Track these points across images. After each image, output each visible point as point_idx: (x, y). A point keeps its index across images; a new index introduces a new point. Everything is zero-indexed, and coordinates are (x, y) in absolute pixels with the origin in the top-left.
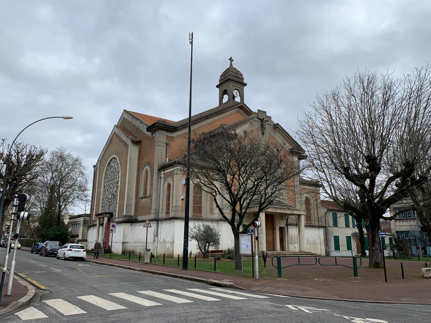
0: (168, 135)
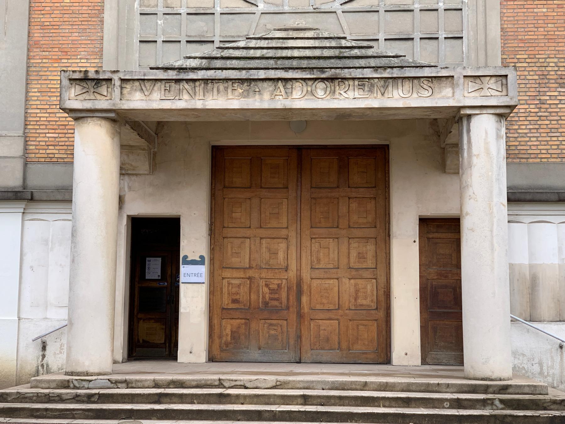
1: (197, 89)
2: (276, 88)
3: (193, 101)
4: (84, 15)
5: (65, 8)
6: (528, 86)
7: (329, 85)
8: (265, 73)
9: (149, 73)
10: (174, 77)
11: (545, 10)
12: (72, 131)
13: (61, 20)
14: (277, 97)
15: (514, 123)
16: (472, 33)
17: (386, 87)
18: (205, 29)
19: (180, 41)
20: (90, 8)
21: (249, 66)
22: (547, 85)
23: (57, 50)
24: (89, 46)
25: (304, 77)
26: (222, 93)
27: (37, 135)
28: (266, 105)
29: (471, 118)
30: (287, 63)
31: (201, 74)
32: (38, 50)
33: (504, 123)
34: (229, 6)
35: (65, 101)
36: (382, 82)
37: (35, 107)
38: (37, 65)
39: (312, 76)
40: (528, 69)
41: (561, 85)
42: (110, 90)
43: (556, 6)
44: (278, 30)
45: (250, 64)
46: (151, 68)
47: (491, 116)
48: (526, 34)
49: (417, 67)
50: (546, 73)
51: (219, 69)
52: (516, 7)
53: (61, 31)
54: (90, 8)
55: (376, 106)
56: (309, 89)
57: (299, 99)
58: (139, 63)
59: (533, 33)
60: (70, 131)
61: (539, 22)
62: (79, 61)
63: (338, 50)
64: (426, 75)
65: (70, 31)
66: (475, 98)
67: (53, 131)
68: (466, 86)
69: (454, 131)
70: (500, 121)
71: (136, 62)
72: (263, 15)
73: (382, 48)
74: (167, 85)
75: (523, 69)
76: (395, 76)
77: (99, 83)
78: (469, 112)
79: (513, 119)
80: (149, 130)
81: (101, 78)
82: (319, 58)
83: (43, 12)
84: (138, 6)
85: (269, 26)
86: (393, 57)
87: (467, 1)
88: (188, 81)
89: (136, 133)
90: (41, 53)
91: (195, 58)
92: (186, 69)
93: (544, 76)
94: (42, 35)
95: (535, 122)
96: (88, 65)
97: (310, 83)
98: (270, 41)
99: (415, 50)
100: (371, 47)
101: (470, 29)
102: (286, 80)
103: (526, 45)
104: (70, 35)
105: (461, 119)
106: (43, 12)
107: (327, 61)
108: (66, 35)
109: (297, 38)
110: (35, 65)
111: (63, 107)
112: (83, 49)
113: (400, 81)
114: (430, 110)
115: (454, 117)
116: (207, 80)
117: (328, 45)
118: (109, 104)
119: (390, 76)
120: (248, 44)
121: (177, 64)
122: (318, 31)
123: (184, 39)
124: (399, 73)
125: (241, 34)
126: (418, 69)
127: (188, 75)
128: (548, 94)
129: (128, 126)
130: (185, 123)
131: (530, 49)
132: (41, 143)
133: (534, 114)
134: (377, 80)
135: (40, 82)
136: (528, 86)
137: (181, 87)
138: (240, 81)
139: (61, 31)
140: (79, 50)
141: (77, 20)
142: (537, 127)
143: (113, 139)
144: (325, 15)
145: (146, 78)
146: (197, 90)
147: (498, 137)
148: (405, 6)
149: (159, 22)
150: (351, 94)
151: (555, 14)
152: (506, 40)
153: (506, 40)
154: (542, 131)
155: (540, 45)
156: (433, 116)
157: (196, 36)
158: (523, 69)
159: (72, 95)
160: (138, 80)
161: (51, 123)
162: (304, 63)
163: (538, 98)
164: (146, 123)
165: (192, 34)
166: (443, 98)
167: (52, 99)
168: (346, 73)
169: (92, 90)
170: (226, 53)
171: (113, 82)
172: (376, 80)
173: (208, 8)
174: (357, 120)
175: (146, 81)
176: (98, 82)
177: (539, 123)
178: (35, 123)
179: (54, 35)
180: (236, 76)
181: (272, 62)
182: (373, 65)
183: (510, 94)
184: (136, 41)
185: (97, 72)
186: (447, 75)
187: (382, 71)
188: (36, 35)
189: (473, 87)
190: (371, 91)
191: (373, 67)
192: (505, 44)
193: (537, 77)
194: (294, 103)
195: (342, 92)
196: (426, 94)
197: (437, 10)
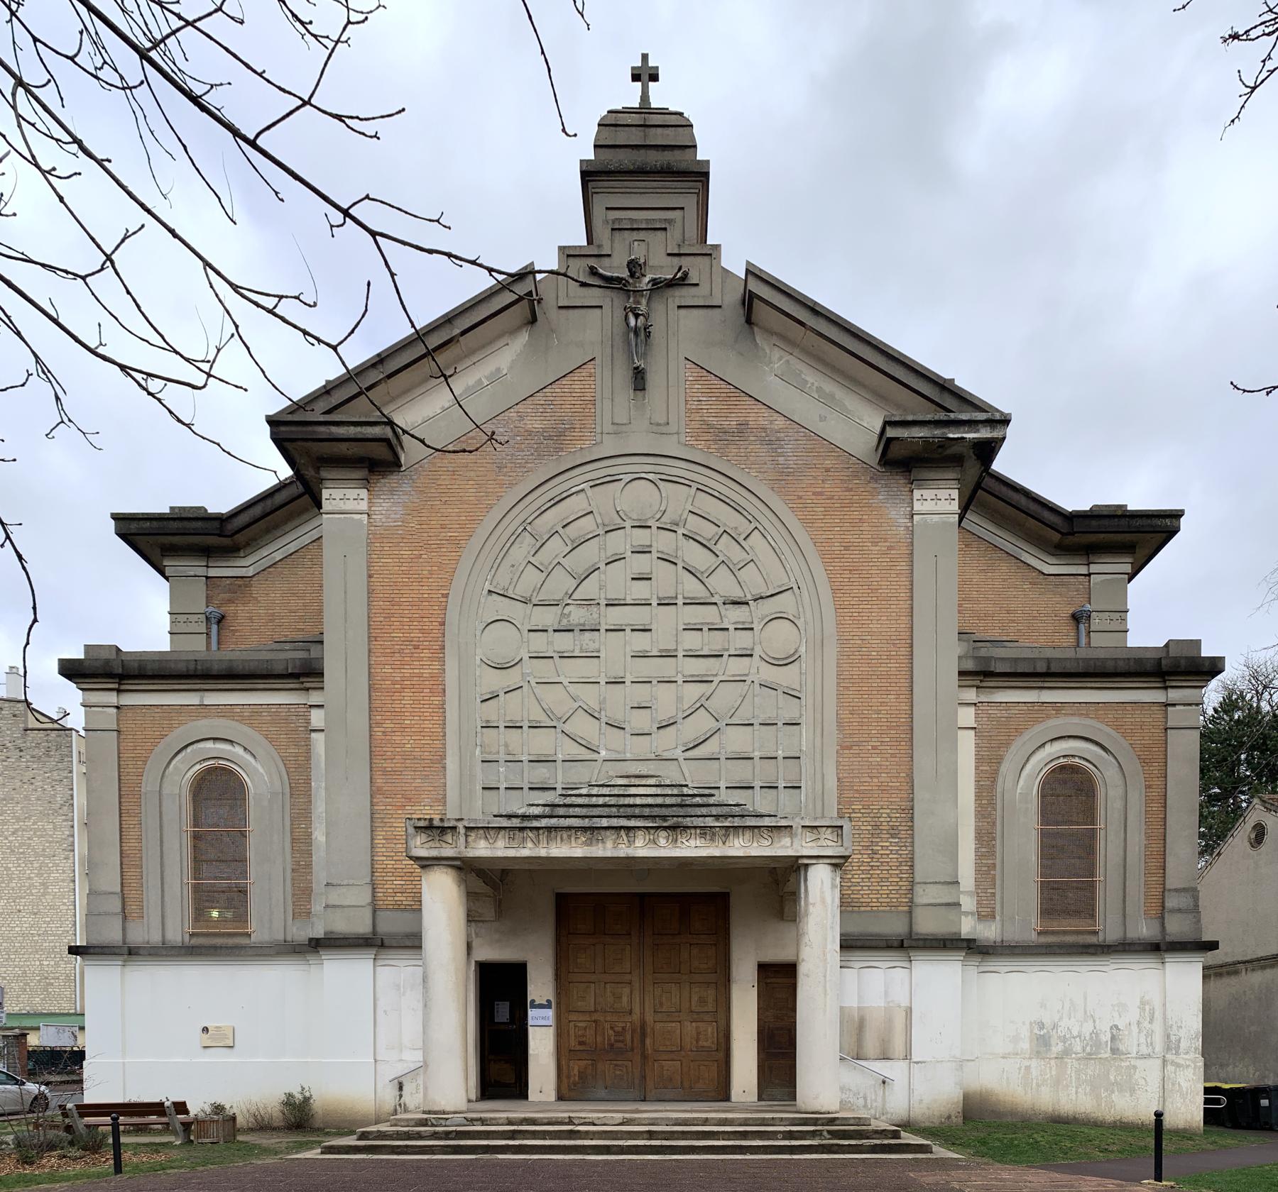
0: (212, 572)
2: (619, 837)
17: (727, 836)
28: (609, 854)
30: (629, 811)
31: (544, 822)
33: (839, 873)
57: (641, 848)
66: (812, 848)
71: (479, 809)
73: (723, 796)
78: (806, 861)
88: (531, 829)
93: (876, 827)
121: (520, 812)
123: (526, 787)
147: (833, 886)
150: (692, 843)
162: (647, 811)
168: (688, 822)
170: (568, 801)
176: (443, 830)
181: (614, 810)
184: (479, 788)
190: (712, 840)
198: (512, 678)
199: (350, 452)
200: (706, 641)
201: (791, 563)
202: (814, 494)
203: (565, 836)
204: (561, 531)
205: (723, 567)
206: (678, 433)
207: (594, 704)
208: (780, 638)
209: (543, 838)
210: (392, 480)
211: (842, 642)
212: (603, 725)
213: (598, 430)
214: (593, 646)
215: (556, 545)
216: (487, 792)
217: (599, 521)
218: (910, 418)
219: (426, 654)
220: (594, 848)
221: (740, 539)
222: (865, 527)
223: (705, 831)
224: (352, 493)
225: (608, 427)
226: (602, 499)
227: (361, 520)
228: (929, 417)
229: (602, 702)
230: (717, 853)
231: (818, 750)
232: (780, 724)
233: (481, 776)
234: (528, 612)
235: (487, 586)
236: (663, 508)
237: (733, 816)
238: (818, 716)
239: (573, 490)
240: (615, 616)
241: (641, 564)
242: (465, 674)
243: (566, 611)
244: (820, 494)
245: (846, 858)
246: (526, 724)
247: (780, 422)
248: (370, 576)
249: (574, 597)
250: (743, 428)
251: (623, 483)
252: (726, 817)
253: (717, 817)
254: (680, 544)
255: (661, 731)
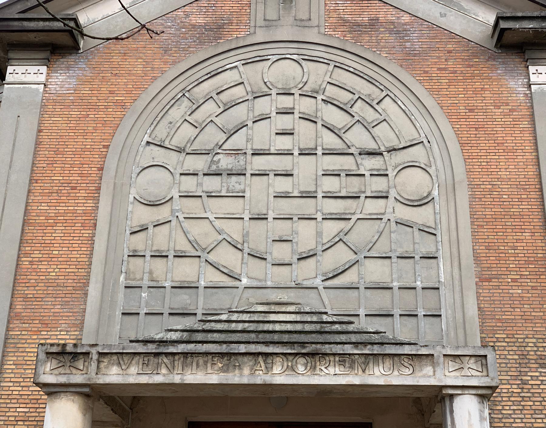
1: (176, 363)
2: (256, 363)
3: (171, 376)
4: (68, 288)
5: (50, 281)
6: (509, 365)
7: (309, 361)
8: (246, 348)
9: (129, 346)
10: (154, 351)
11: (520, 291)
12: (43, 406)
13: (45, 292)
14: (257, 372)
15: (497, 403)
16: (450, 312)
17: (366, 364)
18: (188, 301)
19: (163, 314)
20: (75, 281)
21: (230, 340)
22: (528, 365)
23: (38, 322)
24: (70, 318)
25: (285, 352)
26: (201, 368)
27: (7, 410)
28: (245, 381)
29: (453, 398)
30: (268, 337)
31: (181, 348)
32: (18, 322)
33: (486, 404)
34: (212, 280)
35: (39, 375)
36: (363, 359)
37: (8, 380)
38: (16, 337)
39: (293, 351)
40: (507, 349)
41: (542, 366)
42: (86, 364)
43: (530, 288)
44: (261, 304)
45: (231, 337)
46: (131, 341)
47: (473, 397)
48: (503, 314)
49: (397, 344)
50: (525, 353)
51: (199, 342)
52: (491, 287)
53: (43, 303)
54: (75, 281)
55: (358, 383)
56: (290, 364)
57: (279, 375)
58: (120, 334)
59: (509, 313)
60: (41, 406)
61: (515, 302)
62: (58, 333)
63: (319, 325)
64: (406, 353)
65: (53, 303)
66: (456, 377)
67: (24, 406)
68: (446, 365)
69: (437, 410)
70: (483, 402)
71: (115, 336)
72: (246, 289)
73: (363, 323)
74: (146, 359)
75: (503, 348)
76: (375, 352)
77: (76, 357)
78: (451, 392)
79: (496, 399)
80: (124, 404)
81: (79, 351)
82: (300, 332)
83: (27, 285)
84: (124, 280)
85: (252, 300)
86: (374, 333)
87: (443, 281)
88: (167, 354)
89: (109, 408)
90: (21, 325)
91: (176, 331)
92: (166, 342)
93: (523, 356)
94: (24, 307)
95: (518, 403)
96: (68, 337)
97: (290, 358)
98: (252, 314)
99: (395, 326)
100: (352, 323)
101: (448, 308)
102: (266, 355)
103: (505, 325)
104: (52, 307)
105: (443, 399)
106: (27, 285)
107: (308, 336)
108: (48, 307)
109: (279, 312)
110: (13, 337)
111: (37, 381)
112: (64, 322)
113: (380, 358)
114: (411, 388)
115: (437, 396)
116: (187, 353)
117: (309, 320)
118: (84, 379)
119: (371, 353)
120: (230, 317)
121: (158, 337)
122: (299, 306)
123: (166, 311)
124: (380, 350)
125: (224, 307)
126: (398, 347)
127: (168, 349)
128: (529, 374)
129: (101, 401)
130: (162, 398)
131: (508, 329)
132: (10, 419)
133: (517, 395)
134: (358, 356)
135: (16, 354)
136: (509, 365)
137: (160, 361)
138: (220, 355)
139: (43, 303)
140: (60, 322)
141: (61, 292)
142: (520, 408)
143: (85, 415)
144: (307, 290)
145: (124, 351)
146: (176, 364)
147: (482, 419)
148: (385, 284)
149: (143, 295)
150: (331, 370)
151: (530, 295)
152: (484, 319)
153: (484, 319)
154: (526, 412)
155: (518, 325)
156: (416, 395)
157: (178, 309)
158: (503, 348)
159: (48, 369)
160: (116, 353)
161: (23, 397)
162: (286, 338)
163: (520, 378)
164: (121, 398)
165: (175, 307)
166: (424, 376)
167: (27, 372)
168: (327, 349)
169: (68, 364)
170: (207, 326)
171: (90, 356)
172: (357, 357)
173: (193, 282)
174: (338, 397)
175: (124, 355)
176: (75, 356)
177: (522, 403)
178: (6, 397)
179: (36, 307)
180: (217, 349)
181: (253, 335)
182: (354, 340)
183: (490, 374)
184: (118, 313)
185: (75, 345)
186: (427, 353)
187: (363, 347)
188: (18, 307)
189: (454, 366)
190: (352, 367)
191: (354, 343)
192: (483, 323)
193: (517, 357)
194: (274, 378)
195: (323, 368)
196: (407, 371)
197: (415, 288)
198: (164, 213)
199: (37, 40)
200: (344, 185)
201: (421, 122)
202: (439, 69)
203: (201, 361)
204: (215, 97)
205: (358, 127)
206: (318, 26)
207: (237, 237)
208: (414, 182)
209: (178, 363)
210: (71, 59)
211: (472, 186)
212: (246, 255)
213: (252, 24)
214: (238, 187)
215: (210, 108)
216: (126, 318)
217: (249, 89)
218: (520, 14)
219: (83, 193)
220: (230, 375)
221: (374, 104)
222: (487, 94)
223: (344, 359)
224: (33, 69)
225: (260, 22)
226: (253, 74)
227: (37, 90)
228: (536, 14)
229: (246, 235)
230: (356, 381)
231: (457, 283)
232: (417, 257)
233: (121, 300)
234: (181, 159)
235: (146, 138)
236: (305, 80)
237: (373, 344)
238: (455, 250)
239: (228, 67)
240: (260, 163)
241: (285, 122)
242: (118, 212)
243: (216, 158)
244: (445, 69)
245: (493, 388)
246: (171, 254)
247: (406, 18)
248: (40, 131)
249: (224, 147)
250: (374, 23)
251: (270, 62)
252: (365, 344)
253: (356, 344)
254: (319, 107)
255: (302, 262)
